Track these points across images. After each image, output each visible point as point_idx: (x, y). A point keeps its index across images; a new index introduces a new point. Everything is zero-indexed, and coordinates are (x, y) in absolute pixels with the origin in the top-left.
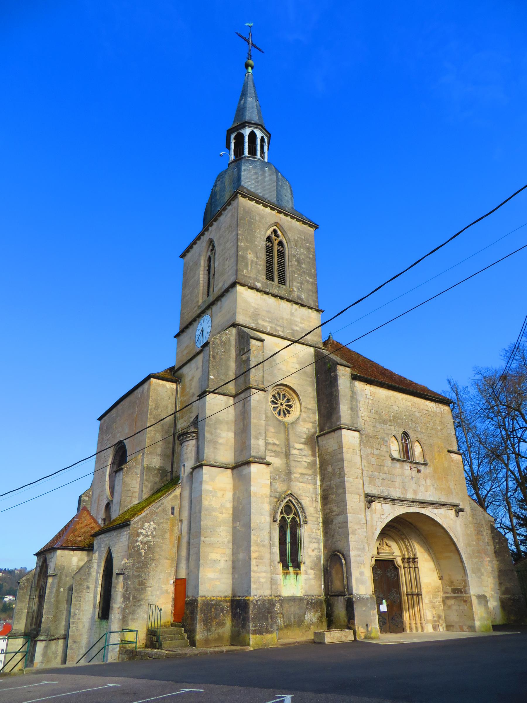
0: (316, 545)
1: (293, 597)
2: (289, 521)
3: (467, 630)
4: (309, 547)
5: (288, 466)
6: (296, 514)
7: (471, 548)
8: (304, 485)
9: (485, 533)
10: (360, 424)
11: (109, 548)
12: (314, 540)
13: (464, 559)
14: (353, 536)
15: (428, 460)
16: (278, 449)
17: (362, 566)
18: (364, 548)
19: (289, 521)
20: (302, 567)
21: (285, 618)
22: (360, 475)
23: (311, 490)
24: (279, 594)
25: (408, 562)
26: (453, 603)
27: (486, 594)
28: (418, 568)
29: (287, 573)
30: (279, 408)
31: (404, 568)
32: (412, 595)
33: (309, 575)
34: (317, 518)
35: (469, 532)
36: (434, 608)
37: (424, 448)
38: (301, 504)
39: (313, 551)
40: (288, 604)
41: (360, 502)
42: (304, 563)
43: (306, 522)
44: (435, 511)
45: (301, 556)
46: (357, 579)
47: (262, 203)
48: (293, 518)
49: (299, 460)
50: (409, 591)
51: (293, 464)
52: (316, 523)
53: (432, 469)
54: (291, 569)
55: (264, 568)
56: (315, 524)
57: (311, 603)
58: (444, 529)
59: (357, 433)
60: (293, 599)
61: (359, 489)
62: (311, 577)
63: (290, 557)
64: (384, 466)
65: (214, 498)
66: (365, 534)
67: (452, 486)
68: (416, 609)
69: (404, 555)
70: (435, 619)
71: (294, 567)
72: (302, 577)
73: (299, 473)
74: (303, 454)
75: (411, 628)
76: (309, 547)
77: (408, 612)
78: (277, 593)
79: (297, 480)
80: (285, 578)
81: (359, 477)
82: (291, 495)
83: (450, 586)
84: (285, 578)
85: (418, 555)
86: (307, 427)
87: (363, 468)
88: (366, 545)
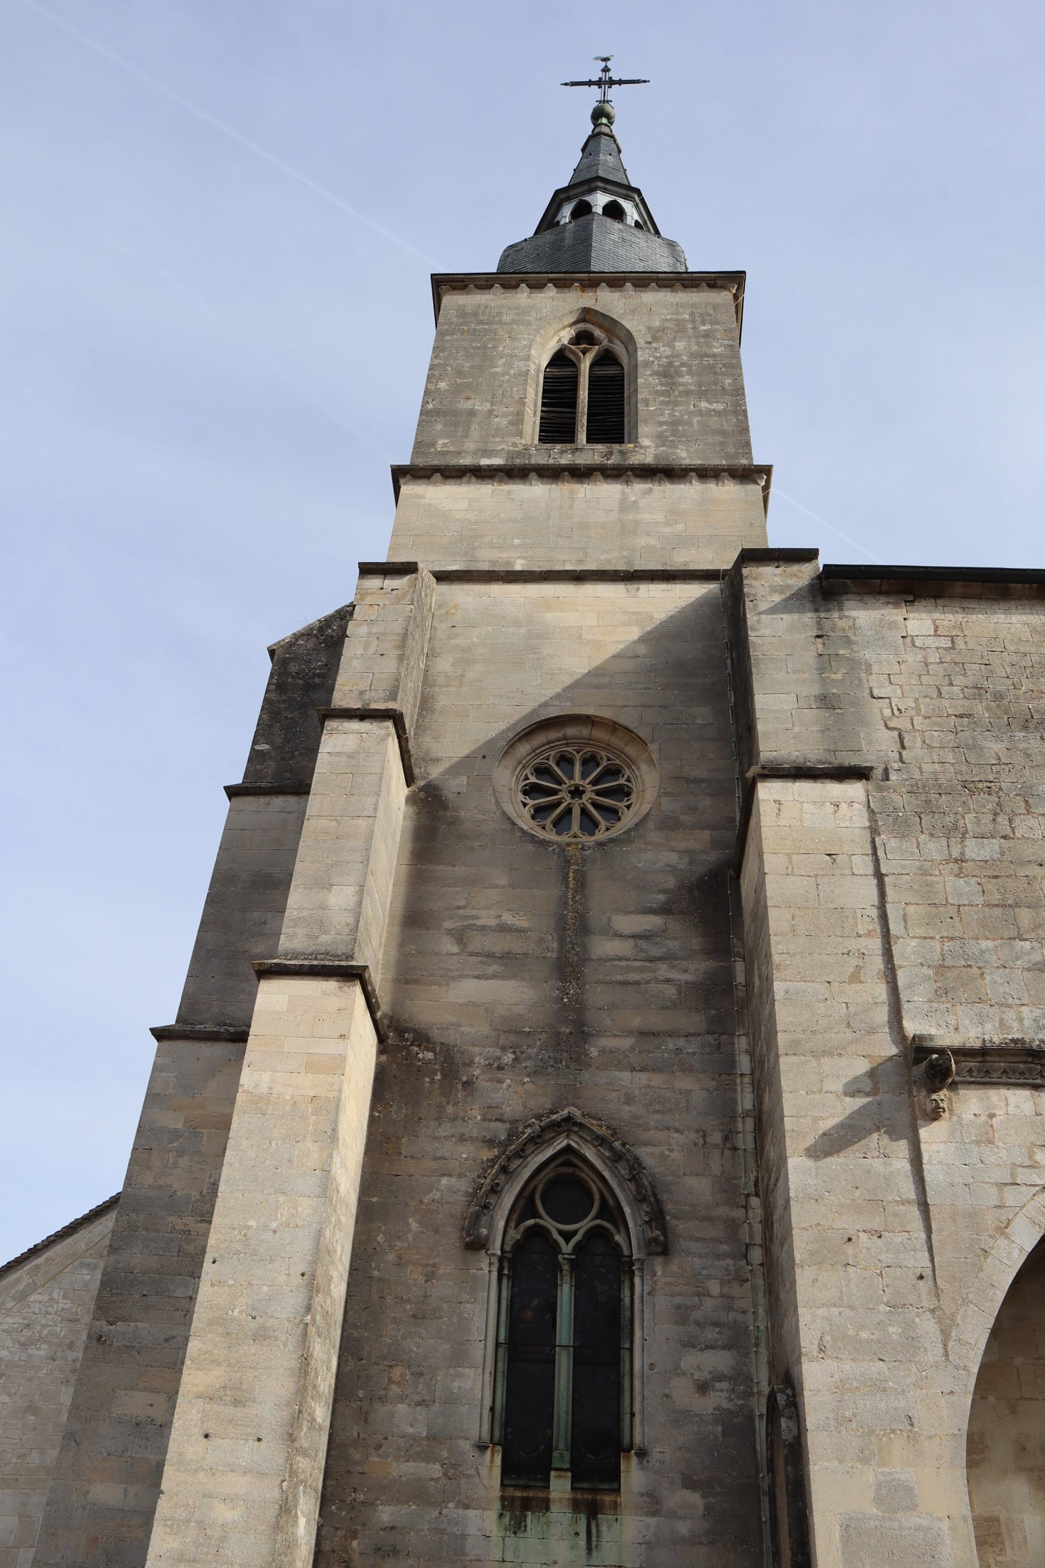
0: (721, 1361)
2: (567, 1248)
4: (677, 1371)
6: (612, 1212)
10: (876, 746)
12: (711, 1334)
16: (515, 945)
18: (911, 1341)
19: (567, 1248)
20: (634, 1476)
23: (699, 1097)
27: (1001, 1518)
29: (527, 1505)
30: (576, 812)
34: (733, 1226)
39: (703, 1388)
42: (642, 1454)
45: (633, 1415)
47: (523, 281)
48: (594, 1233)
49: (633, 977)
52: (725, 1248)
54: (560, 1487)
55: (247, 1452)
56: (719, 1257)
59: (855, 790)
65: (185, 1161)
71: (579, 1474)
72: (627, 1530)
74: (655, 952)
76: (677, 1371)
79: (616, 1060)
80: (517, 1527)
84: (517, 1527)
86: (683, 845)
88: (928, 1326)
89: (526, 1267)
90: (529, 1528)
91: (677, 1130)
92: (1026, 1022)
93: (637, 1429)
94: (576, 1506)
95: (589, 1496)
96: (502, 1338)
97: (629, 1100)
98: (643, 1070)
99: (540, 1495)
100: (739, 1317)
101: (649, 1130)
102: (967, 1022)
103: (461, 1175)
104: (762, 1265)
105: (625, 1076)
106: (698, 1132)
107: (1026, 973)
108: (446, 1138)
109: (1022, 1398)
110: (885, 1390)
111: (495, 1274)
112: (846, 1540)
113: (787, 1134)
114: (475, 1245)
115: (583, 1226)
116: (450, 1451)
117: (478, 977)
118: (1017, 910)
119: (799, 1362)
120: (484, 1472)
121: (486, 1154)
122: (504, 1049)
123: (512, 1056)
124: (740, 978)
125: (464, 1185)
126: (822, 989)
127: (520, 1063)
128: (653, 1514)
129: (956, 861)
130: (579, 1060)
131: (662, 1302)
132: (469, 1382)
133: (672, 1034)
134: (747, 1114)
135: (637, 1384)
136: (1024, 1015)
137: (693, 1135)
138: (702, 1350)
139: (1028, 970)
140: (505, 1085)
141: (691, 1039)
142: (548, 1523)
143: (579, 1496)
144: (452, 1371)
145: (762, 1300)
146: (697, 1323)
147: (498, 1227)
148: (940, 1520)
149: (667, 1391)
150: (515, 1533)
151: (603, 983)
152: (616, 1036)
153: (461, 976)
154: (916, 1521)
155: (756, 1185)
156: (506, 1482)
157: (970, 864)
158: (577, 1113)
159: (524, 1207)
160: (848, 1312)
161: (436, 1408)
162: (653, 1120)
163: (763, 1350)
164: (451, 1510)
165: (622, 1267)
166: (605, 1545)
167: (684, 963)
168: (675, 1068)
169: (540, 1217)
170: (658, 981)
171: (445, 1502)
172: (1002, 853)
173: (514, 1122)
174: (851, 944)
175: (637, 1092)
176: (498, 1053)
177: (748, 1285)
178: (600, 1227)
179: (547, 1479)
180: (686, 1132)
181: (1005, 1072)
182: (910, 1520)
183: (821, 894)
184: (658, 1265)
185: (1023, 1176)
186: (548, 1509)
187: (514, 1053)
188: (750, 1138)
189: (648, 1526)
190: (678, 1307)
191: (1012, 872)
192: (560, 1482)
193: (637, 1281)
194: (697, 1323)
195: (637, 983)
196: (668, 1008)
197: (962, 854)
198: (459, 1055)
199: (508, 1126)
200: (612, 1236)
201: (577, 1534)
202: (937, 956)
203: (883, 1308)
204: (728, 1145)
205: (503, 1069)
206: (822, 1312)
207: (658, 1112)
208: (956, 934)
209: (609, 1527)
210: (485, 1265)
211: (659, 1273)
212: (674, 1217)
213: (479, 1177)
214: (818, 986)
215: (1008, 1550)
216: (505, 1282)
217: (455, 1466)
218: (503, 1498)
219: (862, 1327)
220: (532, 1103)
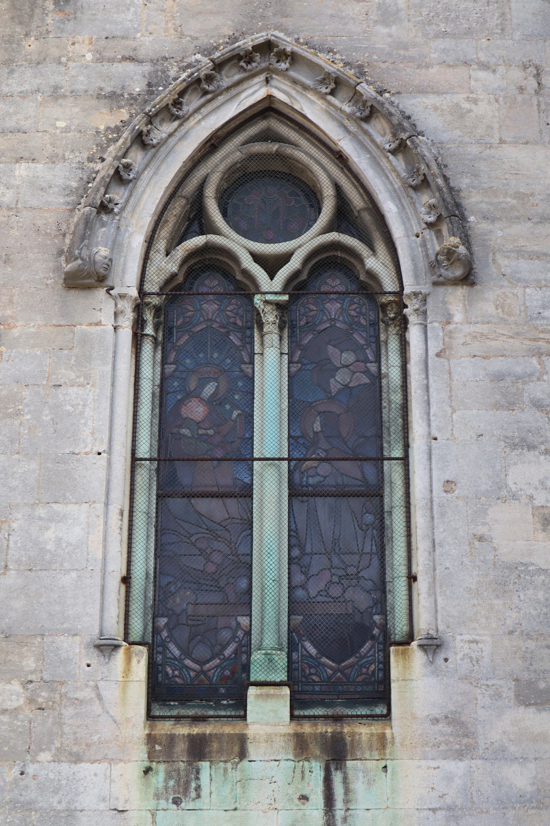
4: (501, 493)
19: (271, 285)
20: (413, 682)
29: (198, 749)
45: (412, 578)
48: (326, 260)
54: (268, 713)
82: (267, 54)
89: (189, 315)
90: (205, 792)
91: (484, 66)
94: (301, 746)
96: (145, 448)
99: (228, 729)
101: (428, 66)
108: (24, 95)
115: (303, 245)
116: (41, 657)
120: (111, 693)
121: (106, 119)
128: (460, 755)
137: (517, 74)
142: (244, 782)
144: (41, 511)
147: (131, 246)
149: (481, 530)
150: (176, 802)
165: (386, 312)
169: (216, 231)
180: (501, 69)
184: (455, 299)
186: (243, 754)
189: (449, 778)
190: (499, 377)
192: (269, 705)
199: (147, 68)
201: (304, 798)
207: (445, 34)
211: (458, 317)
213: (91, 159)
216: (147, 348)
217: (50, 685)
218: (151, 739)
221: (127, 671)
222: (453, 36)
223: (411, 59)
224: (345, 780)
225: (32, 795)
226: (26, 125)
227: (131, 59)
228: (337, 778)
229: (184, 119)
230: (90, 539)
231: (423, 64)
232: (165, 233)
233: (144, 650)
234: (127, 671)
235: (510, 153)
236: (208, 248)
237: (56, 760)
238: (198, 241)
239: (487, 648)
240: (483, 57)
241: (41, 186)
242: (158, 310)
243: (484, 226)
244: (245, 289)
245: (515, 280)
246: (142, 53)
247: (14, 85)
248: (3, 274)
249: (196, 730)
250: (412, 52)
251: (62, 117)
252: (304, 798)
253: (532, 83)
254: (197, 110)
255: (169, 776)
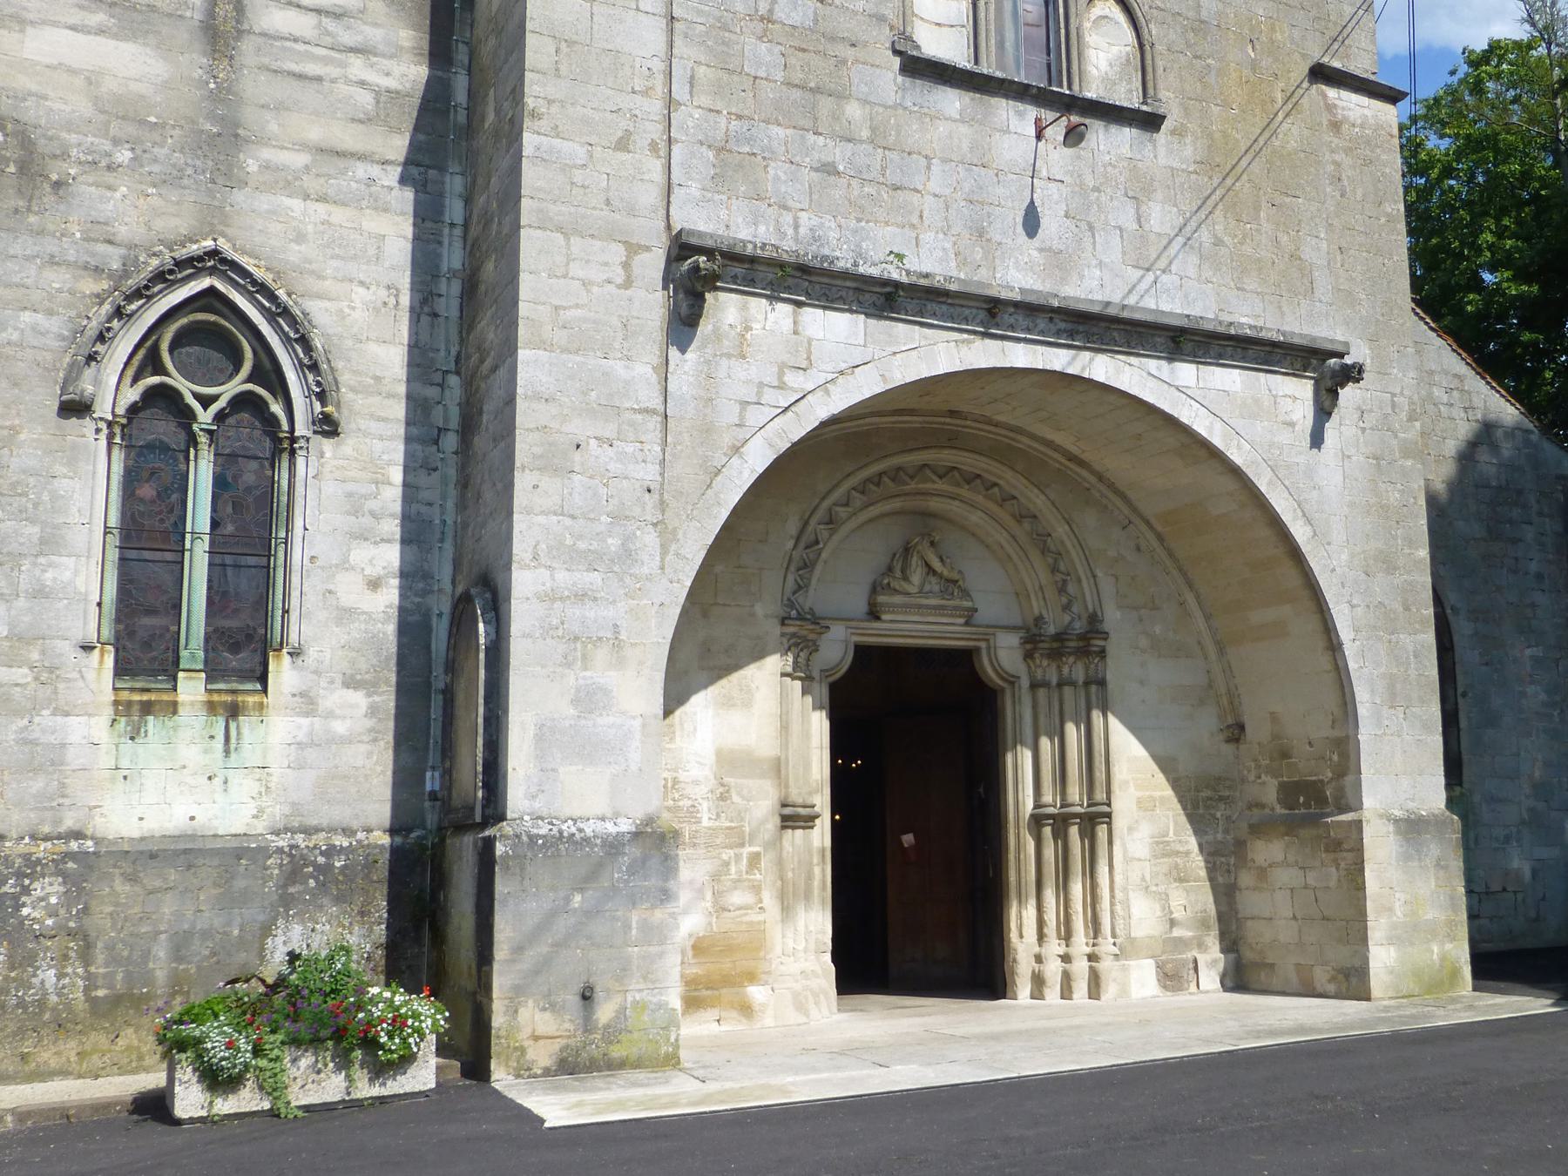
1: (193, 837)
2: (205, 417)
3: (1331, 988)
4: (344, 565)
5: (223, 98)
7: (1399, 579)
8: (339, 215)
9: (1529, 533)
11: (668, 713)
13: (1345, 633)
14: (548, 483)
15: (1168, 101)
17: (601, 655)
18: (628, 554)
19: (205, 417)
20: (282, 673)
21: (100, 956)
22: (655, 131)
24: (69, 823)
25: (1056, 655)
26: (1280, 857)
28: (1102, 683)
29: (147, 708)
31: (1034, 686)
32: (1061, 823)
33: (330, 715)
35: (1394, 497)
36: (1181, 880)
37: (1154, 31)
38: (294, 322)
40: (132, 879)
41: (628, 283)
43: (328, 427)
44: (1186, 372)
45: (286, 612)
46: (544, 736)
48: (242, 402)
49: (311, 69)
50: (1047, 798)
51: (254, 86)
53: (1188, 151)
54: (191, 688)
57: (326, 869)
58: (1235, 471)
60: (179, 855)
61: (632, 212)
62: (340, 727)
63: (192, 612)
64: (841, 96)
66: (650, 473)
67: (1316, 250)
68: (1077, 889)
69: (1039, 620)
70: (1177, 932)
72: (274, 730)
73: (304, 146)
74: (347, 38)
75: (1038, 981)
77: (1032, 902)
78: (58, 821)
79: (287, 182)
81: (642, 142)
82: (216, 261)
83: (1275, 774)
85: (1113, 617)
87: (680, 91)
88: (649, 539)
89: (153, 437)
90: (150, 733)
91: (362, 283)
92: (802, 231)
93: (294, 628)
94: (211, 707)
95: (229, 698)
96: (114, 521)
97: (300, 238)
98: (322, 199)
99: (165, 697)
100: (424, 509)
101: (324, 278)
102: (740, 220)
103: (50, 313)
104: (456, 453)
105: (296, 204)
106: (389, 288)
107: (813, 174)
108: (27, 258)
109: (716, 604)
110: (595, 599)
111: (103, 443)
112: (539, 738)
113: (521, 322)
114: (75, 408)
115: (228, 390)
116: (43, 652)
117: (73, 28)
118: (818, 96)
119: (508, 567)
120: (91, 675)
121: (90, 286)
122: (116, 142)
123: (129, 154)
124: (461, 96)
125: (56, 325)
126: (581, 153)
127: (142, 166)
128: (307, 714)
129: (762, 19)
130: (227, 175)
131: (330, 488)
132: (68, 574)
133: (362, 157)
134: (454, 273)
135: (295, 579)
136: (801, 222)
137: (383, 293)
138: (376, 543)
139: (817, 170)
140: (118, 195)
141: (389, 168)
142: (175, 729)
143: (216, 698)
144: (42, 560)
145: (452, 492)
146: (373, 514)
147: (112, 388)
148: (634, 718)
149: (331, 587)
150: (132, 738)
151: (268, 70)
152: (283, 148)
153: (44, 22)
154: (611, 719)
155: (457, 362)
156: (118, 685)
157: (777, 26)
158: (223, 244)
159: (148, 359)
160: (568, 521)
161: (21, 603)
162: (331, 267)
163: (448, 546)
164: (45, 718)
165: (283, 445)
166: (245, 746)
167: (385, 62)
168: (364, 203)
169: (167, 374)
170: (348, 82)
171: (35, 709)
172: (816, 21)
173: (131, 246)
174: (626, 101)
175: (310, 228)
176: (107, 146)
177: (436, 475)
178: (250, 393)
179: (175, 679)
180: (373, 288)
181: (771, 283)
182: (604, 720)
183: (596, 27)
184: (327, 445)
185: (769, 396)
186: (175, 712)
187: (133, 149)
188: (455, 303)
189: (300, 727)
190: (350, 495)
191: (821, 48)
192: (191, 683)
193: (300, 462)
194: (373, 514)
195: (319, 79)
196: (361, 122)
197: (771, 11)
198: (43, 141)
199: (123, 251)
200: (266, 404)
201: (212, 737)
202: (720, 135)
203: (604, 518)
204: (426, 309)
205: (115, 170)
206: (541, 519)
207: (337, 257)
208: (746, 112)
209: (252, 730)
210: (91, 435)
211: (328, 455)
212: (352, 389)
213: (79, 316)
214: (577, 147)
215: (678, 739)
216: (116, 451)
217: (51, 670)
218: (116, 703)
219: (580, 537)
220: (159, 224)
221: (101, 662)
222: (343, 258)
223: (313, 272)
224: (238, 727)
225: (36, 735)
226: (29, 282)
227: (110, 242)
228: (233, 726)
229: (149, 298)
230: (84, 576)
231: (320, 277)
232: (130, 372)
233: (110, 648)
234: (101, 662)
235: (373, 348)
236: (162, 386)
237: (53, 714)
238: (156, 380)
239: (328, 655)
240: (362, 277)
241: (42, 330)
242: (123, 426)
243: (351, 395)
244: (187, 415)
245: (366, 434)
246: (118, 239)
247: (16, 249)
248: (1066, 992)
249: (145, 697)
250: (314, 266)
251: (57, 279)
252: (212, 737)
253: (392, 301)
254: (160, 292)
255: (127, 724)
